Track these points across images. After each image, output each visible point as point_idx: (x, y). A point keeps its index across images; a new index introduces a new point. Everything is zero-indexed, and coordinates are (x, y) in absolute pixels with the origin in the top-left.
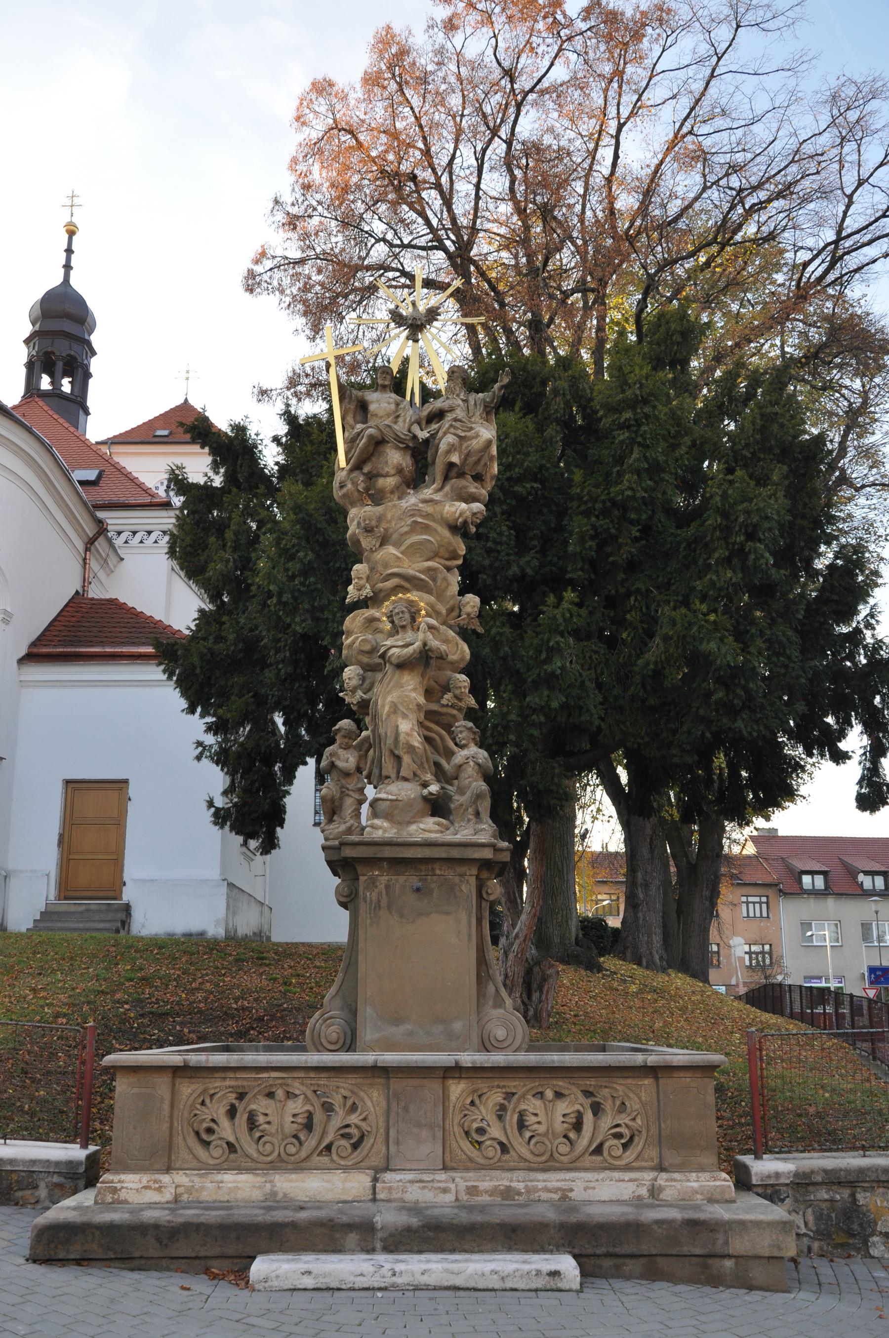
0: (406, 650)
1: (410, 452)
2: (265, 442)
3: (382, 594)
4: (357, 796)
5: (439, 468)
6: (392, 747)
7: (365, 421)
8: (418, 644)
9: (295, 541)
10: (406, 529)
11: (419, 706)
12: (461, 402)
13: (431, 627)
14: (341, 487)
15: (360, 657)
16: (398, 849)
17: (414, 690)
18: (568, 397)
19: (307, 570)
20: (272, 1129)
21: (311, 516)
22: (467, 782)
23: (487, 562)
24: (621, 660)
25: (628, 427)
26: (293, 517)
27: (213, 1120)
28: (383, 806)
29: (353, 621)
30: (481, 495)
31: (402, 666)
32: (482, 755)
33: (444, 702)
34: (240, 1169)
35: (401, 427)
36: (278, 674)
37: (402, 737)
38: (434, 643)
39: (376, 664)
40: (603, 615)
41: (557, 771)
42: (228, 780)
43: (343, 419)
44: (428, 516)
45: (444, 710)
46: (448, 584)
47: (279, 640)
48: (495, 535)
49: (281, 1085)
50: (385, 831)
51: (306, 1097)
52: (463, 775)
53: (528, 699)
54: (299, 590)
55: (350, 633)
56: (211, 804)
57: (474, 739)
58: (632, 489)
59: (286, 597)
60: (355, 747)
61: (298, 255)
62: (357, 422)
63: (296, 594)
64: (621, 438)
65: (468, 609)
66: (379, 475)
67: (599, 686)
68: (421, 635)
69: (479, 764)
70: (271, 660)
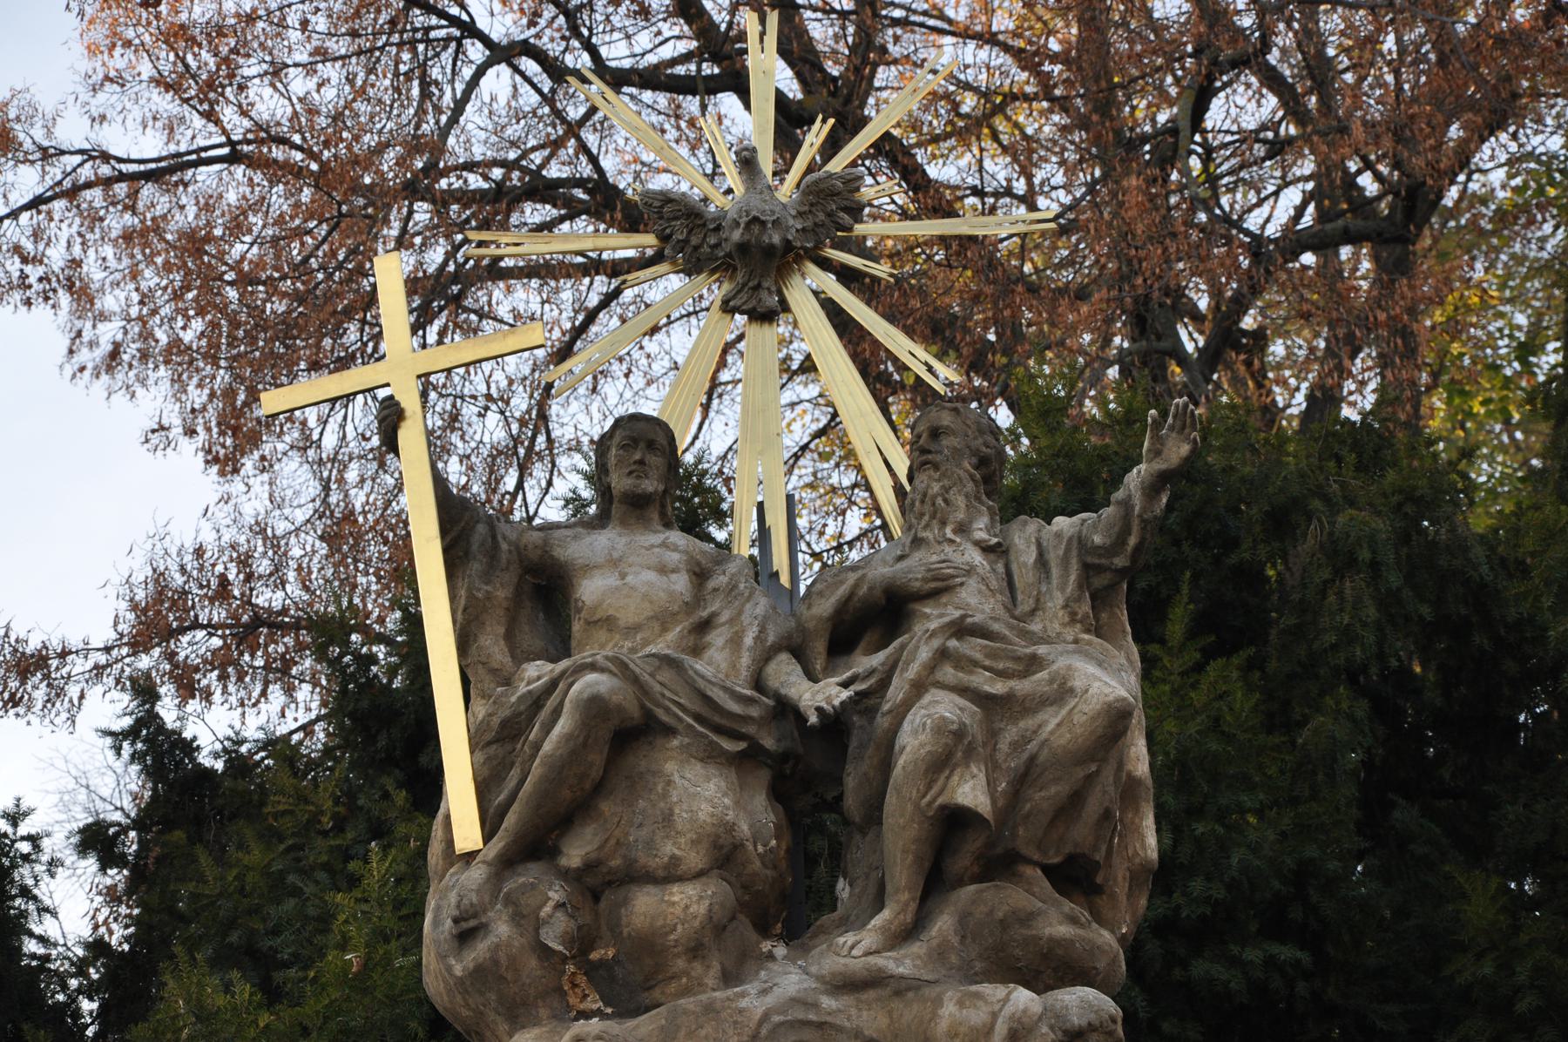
1: (764, 775)
7: (560, 646)
12: (977, 557)
14: (465, 937)
18: (1394, 579)
30: (1094, 949)
43: (464, 643)
61: (151, 146)
62: (521, 657)
66: (636, 876)
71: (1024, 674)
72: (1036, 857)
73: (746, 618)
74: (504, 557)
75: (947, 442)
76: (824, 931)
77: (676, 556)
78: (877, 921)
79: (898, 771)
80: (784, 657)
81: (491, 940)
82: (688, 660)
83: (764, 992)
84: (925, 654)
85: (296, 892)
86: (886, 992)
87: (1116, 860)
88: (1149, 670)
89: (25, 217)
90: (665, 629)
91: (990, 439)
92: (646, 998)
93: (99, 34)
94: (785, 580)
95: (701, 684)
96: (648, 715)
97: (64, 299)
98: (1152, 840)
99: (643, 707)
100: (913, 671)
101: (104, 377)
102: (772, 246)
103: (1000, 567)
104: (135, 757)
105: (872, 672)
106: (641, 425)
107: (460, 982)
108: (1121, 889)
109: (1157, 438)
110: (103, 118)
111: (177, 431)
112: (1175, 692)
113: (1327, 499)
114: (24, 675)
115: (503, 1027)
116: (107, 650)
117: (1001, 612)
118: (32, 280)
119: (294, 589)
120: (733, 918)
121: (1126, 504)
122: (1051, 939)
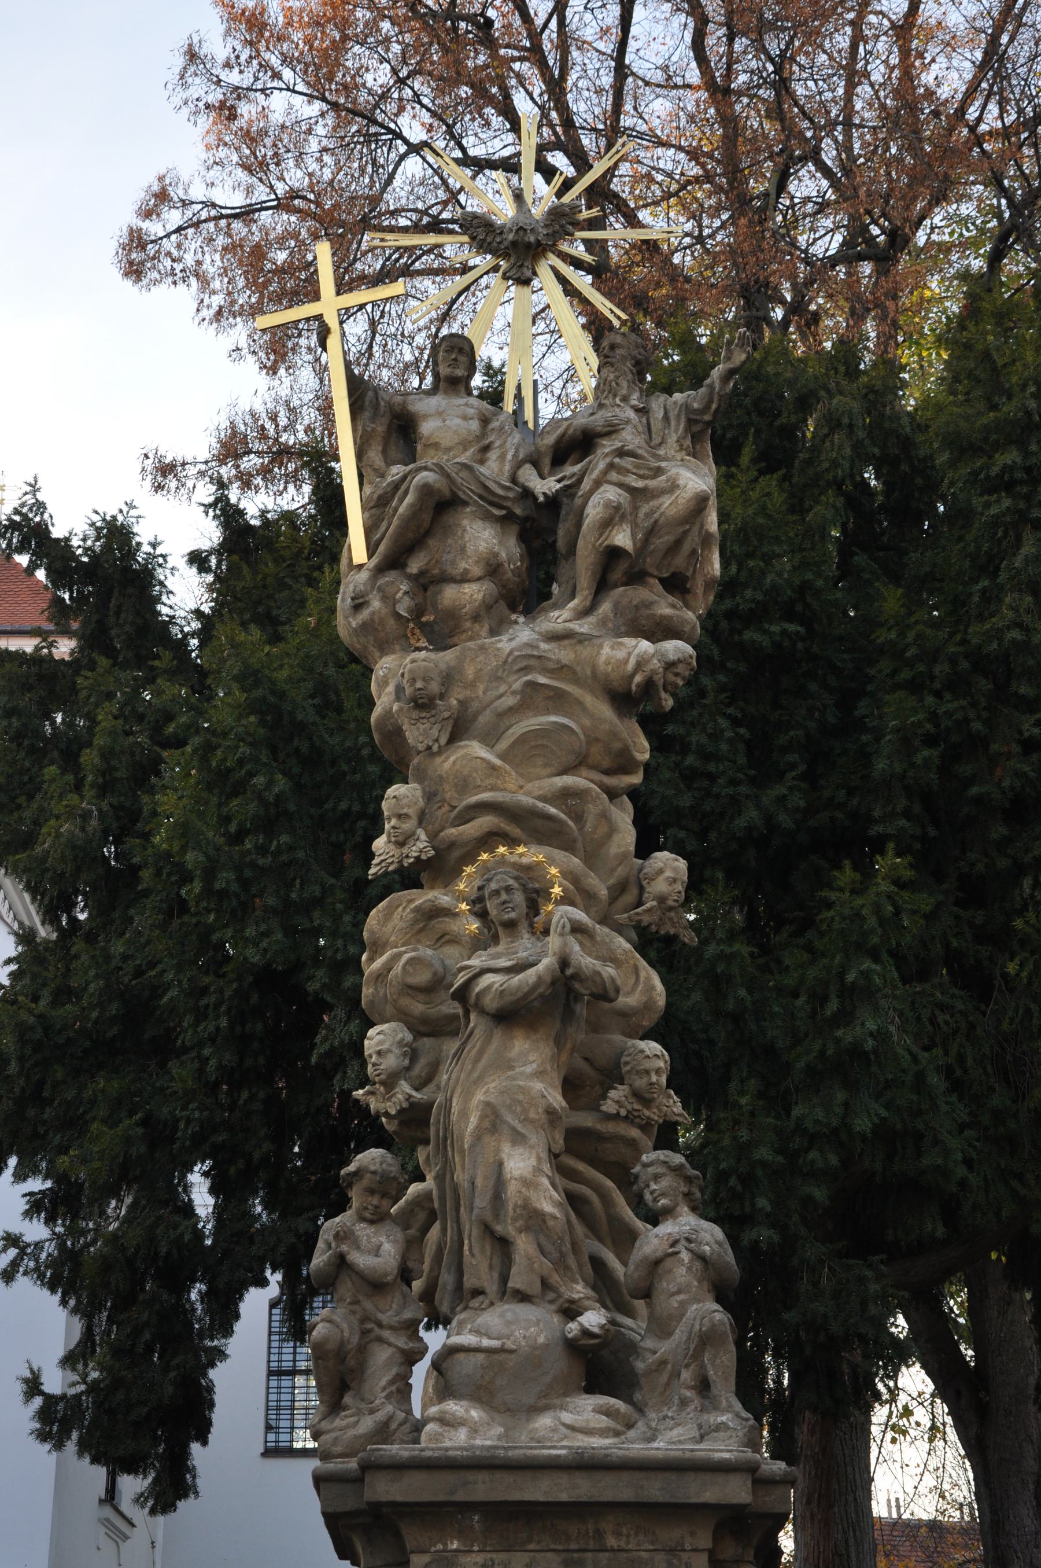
0: (517, 979)
1: (515, 529)
2: (171, 562)
3: (456, 854)
4: (402, 1342)
5: (584, 563)
6: (489, 1217)
8: (547, 963)
9: (244, 750)
10: (510, 701)
11: (551, 1113)
12: (631, 414)
13: (577, 929)
15: (405, 1002)
16: (510, 1478)
17: (539, 1074)
18: (861, 434)
19: (269, 822)
21: (282, 695)
22: (674, 1302)
23: (686, 801)
24: (1005, 1026)
25: (1009, 487)
26: (240, 696)
28: (467, 1364)
29: (387, 919)
30: (684, 621)
31: (511, 1016)
32: (711, 1235)
33: (609, 1107)
35: (494, 470)
36: (201, 1071)
37: (512, 1190)
38: (584, 960)
39: (443, 1015)
40: (957, 917)
41: (873, 1287)
42: (78, 1326)
43: (360, 455)
44: (561, 670)
45: (609, 1128)
46: (612, 830)
47: (204, 991)
48: (704, 739)
50: (474, 1431)
52: (665, 1285)
53: (797, 1112)
54: (253, 865)
55: (378, 947)
56: (33, 1386)
57: (687, 1195)
58: (1019, 625)
59: (225, 879)
60: (395, 1220)
61: (237, 200)
62: (389, 462)
63: (248, 873)
64: (994, 510)
65: (660, 886)
67: (956, 1086)
68: (554, 942)
69: (702, 1258)
70: (187, 1038)
71: (654, 477)
72: (655, 573)
73: (508, 445)
74: (382, 409)
75: (619, 352)
76: (545, 611)
77: (472, 411)
78: (571, 605)
79: (584, 527)
80: (528, 466)
81: (371, 609)
82: (476, 466)
83: (511, 640)
84: (602, 465)
85: (290, 588)
86: (572, 641)
87: (698, 576)
88: (725, 481)
89: (173, 237)
90: (465, 450)
91: (641, 350)
92: (450, 641)
93: (212, 139)
94: (531, 425)
95: (483, 479)
96: (454, 494)
97: (193, 281)
98: (717, 566)
99: (451, 490)
100: (595, 474)
101: (215, 325)
102: (530, 243)
103: (644, 420)
104: (215, 517)
105: (574, 474)
106: (456, 339)
107: (355, 630)
108: (700, 591)
109: (729, 351)
110: (213, 184)
111: (245, 351)
112: (743, 492)
113: (828, 391)
114: (164, 476)
115: (377, 654)
116: (206, 462)
117: (644, 444)
118: (177, 271)
119: (301, 435)
120: (496, 602)
121: (711, 387)
122: (661, 616)
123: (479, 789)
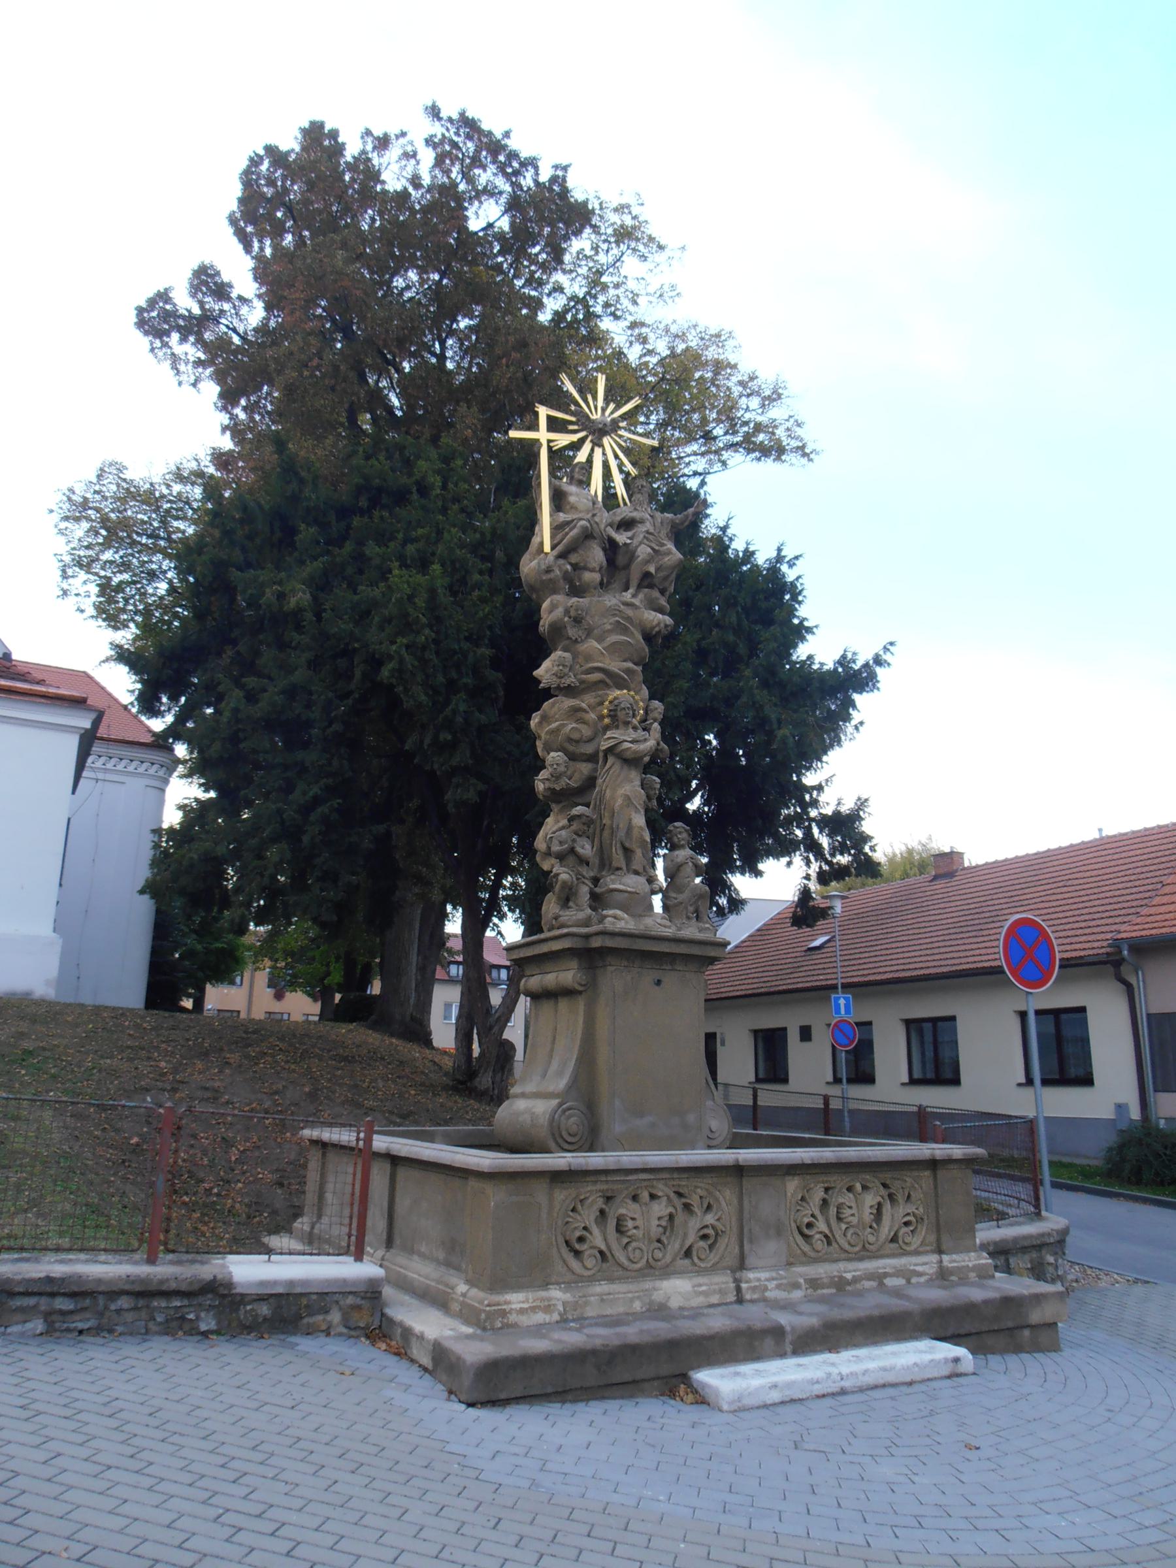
10: (608, 627)
20: (639, 1233)
27: (585, 1228)
34: (611, 1280)
44: (628, 619)
49: (646, 1187)
51: (668, 1197)
66: (585, 568)
123: (594, 661)
